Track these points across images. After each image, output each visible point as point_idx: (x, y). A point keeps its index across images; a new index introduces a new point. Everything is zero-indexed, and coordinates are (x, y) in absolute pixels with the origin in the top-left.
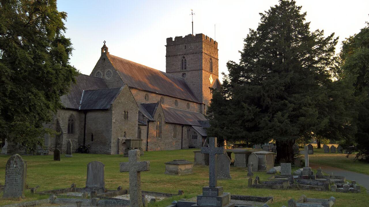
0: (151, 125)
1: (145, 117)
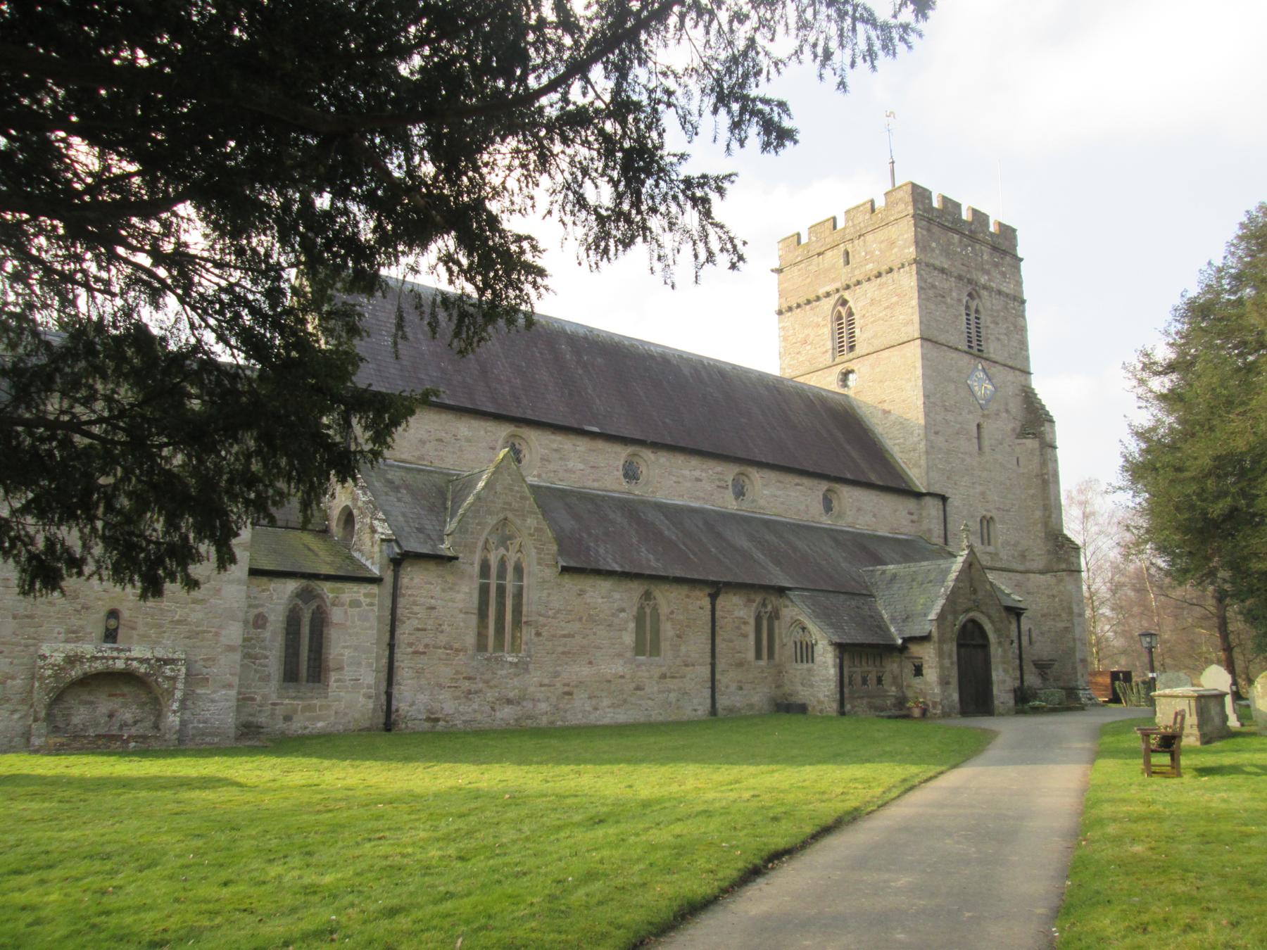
0: (416, 580)
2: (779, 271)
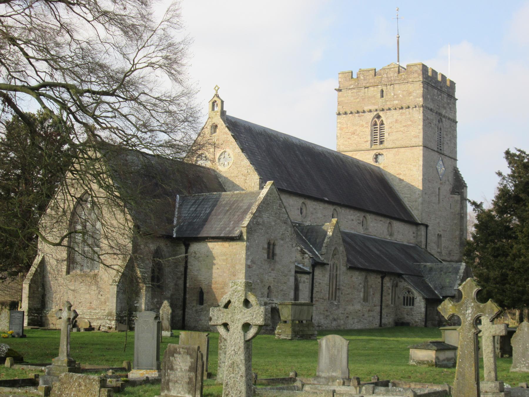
0: (318, 272)
1: (307, 256)
2: (339, 90)
